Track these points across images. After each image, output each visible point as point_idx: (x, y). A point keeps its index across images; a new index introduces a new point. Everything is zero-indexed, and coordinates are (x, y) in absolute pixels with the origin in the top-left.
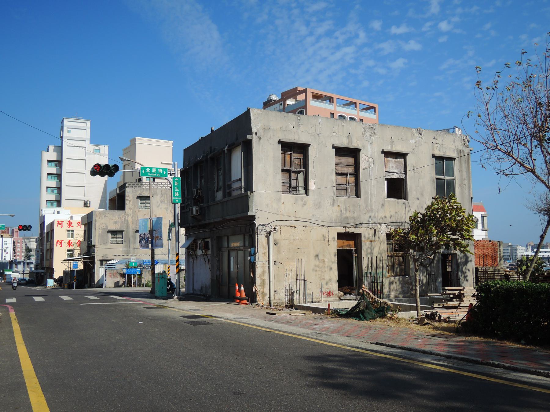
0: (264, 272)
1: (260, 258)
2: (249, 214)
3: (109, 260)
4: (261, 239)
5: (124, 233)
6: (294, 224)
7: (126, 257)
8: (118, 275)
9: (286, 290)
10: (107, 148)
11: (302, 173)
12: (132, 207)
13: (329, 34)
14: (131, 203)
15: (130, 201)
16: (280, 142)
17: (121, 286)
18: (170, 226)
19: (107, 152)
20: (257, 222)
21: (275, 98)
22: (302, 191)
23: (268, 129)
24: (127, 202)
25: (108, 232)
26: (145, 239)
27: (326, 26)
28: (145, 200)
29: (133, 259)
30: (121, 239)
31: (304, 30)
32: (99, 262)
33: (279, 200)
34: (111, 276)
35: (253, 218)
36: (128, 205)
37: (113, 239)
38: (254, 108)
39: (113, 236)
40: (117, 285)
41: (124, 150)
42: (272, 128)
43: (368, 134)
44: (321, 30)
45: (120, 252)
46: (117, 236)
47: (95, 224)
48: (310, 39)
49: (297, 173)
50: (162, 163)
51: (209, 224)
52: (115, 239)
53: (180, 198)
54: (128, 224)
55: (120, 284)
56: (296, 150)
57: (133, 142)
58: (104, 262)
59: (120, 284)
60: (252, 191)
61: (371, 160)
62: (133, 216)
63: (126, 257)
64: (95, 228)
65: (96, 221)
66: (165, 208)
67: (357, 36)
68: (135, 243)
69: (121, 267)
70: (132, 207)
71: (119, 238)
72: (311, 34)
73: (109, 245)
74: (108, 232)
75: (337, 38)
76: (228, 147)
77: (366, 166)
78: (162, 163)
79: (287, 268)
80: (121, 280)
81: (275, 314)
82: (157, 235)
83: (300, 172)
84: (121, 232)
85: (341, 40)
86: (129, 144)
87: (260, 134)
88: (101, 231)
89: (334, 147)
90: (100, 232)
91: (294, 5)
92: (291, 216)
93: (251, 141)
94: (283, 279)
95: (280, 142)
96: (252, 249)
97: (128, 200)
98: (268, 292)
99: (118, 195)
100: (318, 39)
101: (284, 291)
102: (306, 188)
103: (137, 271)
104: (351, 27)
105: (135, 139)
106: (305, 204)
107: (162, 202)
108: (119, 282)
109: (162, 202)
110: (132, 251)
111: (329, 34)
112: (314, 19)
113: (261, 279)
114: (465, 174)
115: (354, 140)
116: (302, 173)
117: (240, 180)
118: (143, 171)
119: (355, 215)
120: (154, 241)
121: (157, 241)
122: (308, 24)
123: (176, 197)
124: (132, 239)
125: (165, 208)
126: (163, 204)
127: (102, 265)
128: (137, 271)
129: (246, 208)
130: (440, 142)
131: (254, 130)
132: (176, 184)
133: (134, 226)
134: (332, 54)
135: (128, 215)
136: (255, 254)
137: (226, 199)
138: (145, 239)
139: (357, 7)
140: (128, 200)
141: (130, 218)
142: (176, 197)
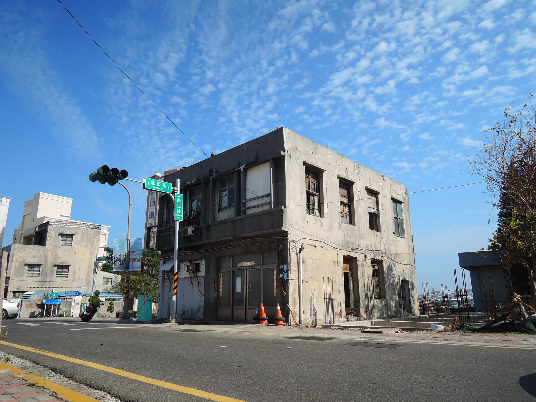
0: (295, 291)
1: (292, 276)
2: (284, 229)
3: (25, 292)
4: (293, 257)
5: (41, 266)
6: (315, 243)
7: (41, 289)
8: (35, 306)
9: (311, 310)
10: (9, 200)
11: (316, 197)
12: (53, 243)
13: (175, 149)
14: (52, 239)
15: (51, 238)
16: (305, 163)
17: (36, 317)
18: (97, 260)
19: (8, 204)
20: (290, 237)
21: (159, 174)
22: (317, 213)
23: (295, 149)
24: (48, 238)
25: (26, 265)
26: (120, 261)
27: (175, 143)
28: (67, 237)
29: (55, 290)
30: (38, 272)
31: (159, 144)
32: (12, 294)
33: (305, 218)
34: (27, 307)
35: (286, 233)
36: (49, 241)
37: (29, 272)
38: (286, 127)
39: (30, 269)
40: (32, 315)
41: (25, 203)
42: (298, 149)
43: (356, 172)
44: (170, 146)
45: (35, 284)
46: (34, 269)
47: (12, 257)
48: (162, 150)
49: (313, 195)
50: (61, 216)
51: (204, 245)
52: (32, 272)
53: (182, 216)
54: (47, 258)
55: (36, 314)
56: (314, 173)
57: (37, 197)
58: (17, 294)
59: (36, 314)
60: (285, 206)
61: (360, 194)
62: (52, 252)
63: (41, 289)
64: (12, 261)
65: (13, 254)
66: (85, 246)
67: (194, 152)
68: (51, 276)
69: (35, 297)
70: (53, 243)
71: (36, 271)
72: (164, 147)
73: (25, 278)
74: (26, 265)
75: (181, 152)
76: (246, 166)
77: (358, 199)
78: (61, 216)
79: (311, 287)
80: (38, 311)
81: (381, 332)
82: (134, 257)
83: (315, 195)
84: (39, 265)
85: (183, 153)
86: (32, 198)
87: (291, 152)
88: (17, 264)
89: (338, 177)
90: (17, 265)
91: (153, 127)
92: (313, 236)
93: (283, 157)
94: (309, 299)
95: (305, 163)
96: (285, 266)
97: (49, 236)
98: (298, 312)
99: (37, 233)
100: (168, 152)
101: (310, 311)
102: (321, 210)
103: (58, 301)
104: (191, 146)
105: (39, 194)
106: (322, 225)
107: (82, 240)
108: (34, 312)
109: (82, 240)
110: (48, 283)
111: (175, 149)
112: (167, 138)
113: (293, 298)
114: (407, 216)
115: (350, 175)
116: (316, 197)
117: (269, 195)
118: (149, 183)
119: (353, 241)
120: (131, 263)
121: (135, 263)
122: (161, 141)
123: (178, 213)
124: (49, 273)
125: (85, 246)
126: (83, 243)
127: (14, 296)
128: (58, 301)
129: (280, 221)
130: (394, 188)
131: (286, 148)
132: (178, 201)
133: (52, 261)
134: (178, 161)
135: (48, 250)
136: (287, 272)
137: (240, 217)
138: (120, 261)
139: (196, 134)
140: (49, 236)
141: (49, 254)
142: (178, 213)
